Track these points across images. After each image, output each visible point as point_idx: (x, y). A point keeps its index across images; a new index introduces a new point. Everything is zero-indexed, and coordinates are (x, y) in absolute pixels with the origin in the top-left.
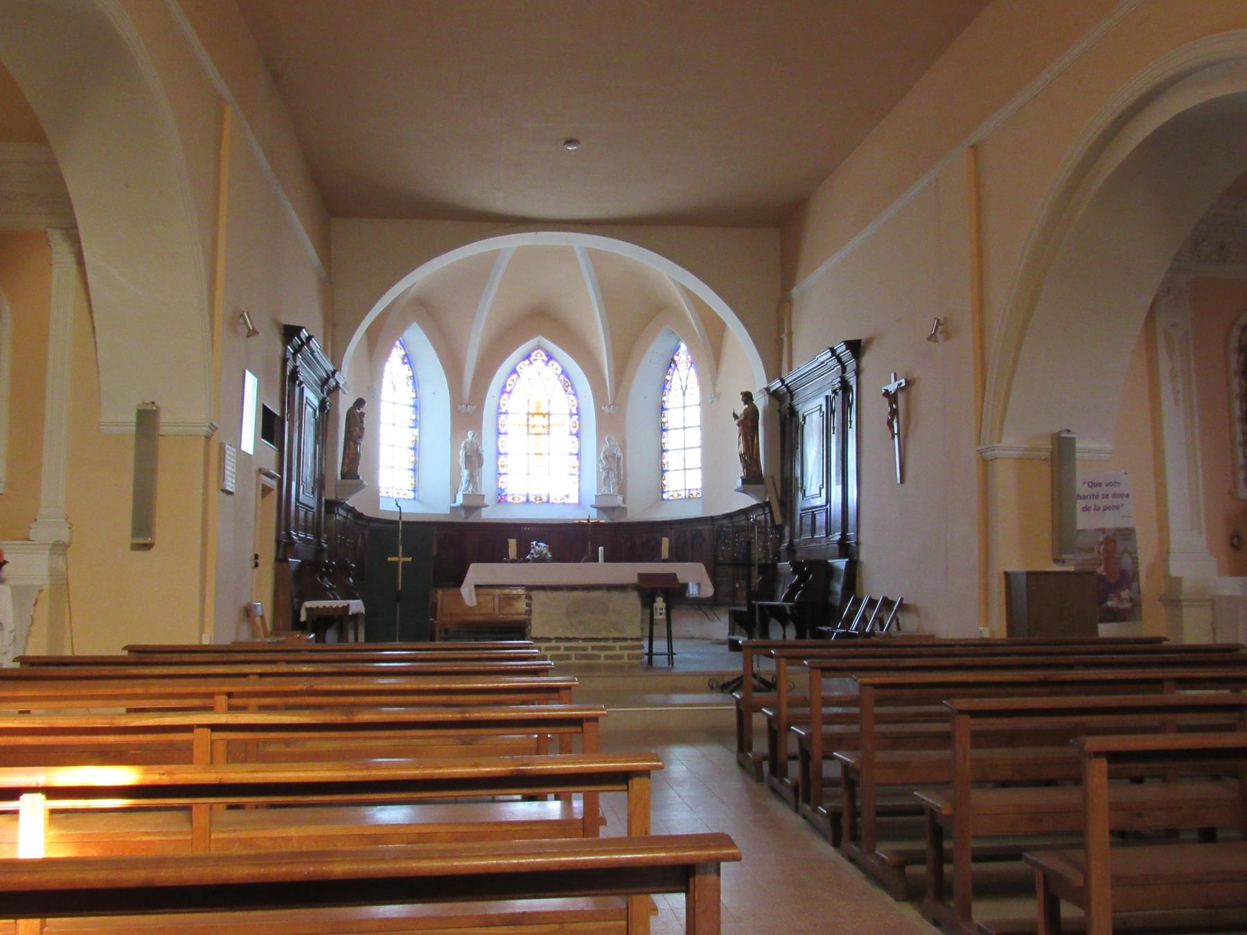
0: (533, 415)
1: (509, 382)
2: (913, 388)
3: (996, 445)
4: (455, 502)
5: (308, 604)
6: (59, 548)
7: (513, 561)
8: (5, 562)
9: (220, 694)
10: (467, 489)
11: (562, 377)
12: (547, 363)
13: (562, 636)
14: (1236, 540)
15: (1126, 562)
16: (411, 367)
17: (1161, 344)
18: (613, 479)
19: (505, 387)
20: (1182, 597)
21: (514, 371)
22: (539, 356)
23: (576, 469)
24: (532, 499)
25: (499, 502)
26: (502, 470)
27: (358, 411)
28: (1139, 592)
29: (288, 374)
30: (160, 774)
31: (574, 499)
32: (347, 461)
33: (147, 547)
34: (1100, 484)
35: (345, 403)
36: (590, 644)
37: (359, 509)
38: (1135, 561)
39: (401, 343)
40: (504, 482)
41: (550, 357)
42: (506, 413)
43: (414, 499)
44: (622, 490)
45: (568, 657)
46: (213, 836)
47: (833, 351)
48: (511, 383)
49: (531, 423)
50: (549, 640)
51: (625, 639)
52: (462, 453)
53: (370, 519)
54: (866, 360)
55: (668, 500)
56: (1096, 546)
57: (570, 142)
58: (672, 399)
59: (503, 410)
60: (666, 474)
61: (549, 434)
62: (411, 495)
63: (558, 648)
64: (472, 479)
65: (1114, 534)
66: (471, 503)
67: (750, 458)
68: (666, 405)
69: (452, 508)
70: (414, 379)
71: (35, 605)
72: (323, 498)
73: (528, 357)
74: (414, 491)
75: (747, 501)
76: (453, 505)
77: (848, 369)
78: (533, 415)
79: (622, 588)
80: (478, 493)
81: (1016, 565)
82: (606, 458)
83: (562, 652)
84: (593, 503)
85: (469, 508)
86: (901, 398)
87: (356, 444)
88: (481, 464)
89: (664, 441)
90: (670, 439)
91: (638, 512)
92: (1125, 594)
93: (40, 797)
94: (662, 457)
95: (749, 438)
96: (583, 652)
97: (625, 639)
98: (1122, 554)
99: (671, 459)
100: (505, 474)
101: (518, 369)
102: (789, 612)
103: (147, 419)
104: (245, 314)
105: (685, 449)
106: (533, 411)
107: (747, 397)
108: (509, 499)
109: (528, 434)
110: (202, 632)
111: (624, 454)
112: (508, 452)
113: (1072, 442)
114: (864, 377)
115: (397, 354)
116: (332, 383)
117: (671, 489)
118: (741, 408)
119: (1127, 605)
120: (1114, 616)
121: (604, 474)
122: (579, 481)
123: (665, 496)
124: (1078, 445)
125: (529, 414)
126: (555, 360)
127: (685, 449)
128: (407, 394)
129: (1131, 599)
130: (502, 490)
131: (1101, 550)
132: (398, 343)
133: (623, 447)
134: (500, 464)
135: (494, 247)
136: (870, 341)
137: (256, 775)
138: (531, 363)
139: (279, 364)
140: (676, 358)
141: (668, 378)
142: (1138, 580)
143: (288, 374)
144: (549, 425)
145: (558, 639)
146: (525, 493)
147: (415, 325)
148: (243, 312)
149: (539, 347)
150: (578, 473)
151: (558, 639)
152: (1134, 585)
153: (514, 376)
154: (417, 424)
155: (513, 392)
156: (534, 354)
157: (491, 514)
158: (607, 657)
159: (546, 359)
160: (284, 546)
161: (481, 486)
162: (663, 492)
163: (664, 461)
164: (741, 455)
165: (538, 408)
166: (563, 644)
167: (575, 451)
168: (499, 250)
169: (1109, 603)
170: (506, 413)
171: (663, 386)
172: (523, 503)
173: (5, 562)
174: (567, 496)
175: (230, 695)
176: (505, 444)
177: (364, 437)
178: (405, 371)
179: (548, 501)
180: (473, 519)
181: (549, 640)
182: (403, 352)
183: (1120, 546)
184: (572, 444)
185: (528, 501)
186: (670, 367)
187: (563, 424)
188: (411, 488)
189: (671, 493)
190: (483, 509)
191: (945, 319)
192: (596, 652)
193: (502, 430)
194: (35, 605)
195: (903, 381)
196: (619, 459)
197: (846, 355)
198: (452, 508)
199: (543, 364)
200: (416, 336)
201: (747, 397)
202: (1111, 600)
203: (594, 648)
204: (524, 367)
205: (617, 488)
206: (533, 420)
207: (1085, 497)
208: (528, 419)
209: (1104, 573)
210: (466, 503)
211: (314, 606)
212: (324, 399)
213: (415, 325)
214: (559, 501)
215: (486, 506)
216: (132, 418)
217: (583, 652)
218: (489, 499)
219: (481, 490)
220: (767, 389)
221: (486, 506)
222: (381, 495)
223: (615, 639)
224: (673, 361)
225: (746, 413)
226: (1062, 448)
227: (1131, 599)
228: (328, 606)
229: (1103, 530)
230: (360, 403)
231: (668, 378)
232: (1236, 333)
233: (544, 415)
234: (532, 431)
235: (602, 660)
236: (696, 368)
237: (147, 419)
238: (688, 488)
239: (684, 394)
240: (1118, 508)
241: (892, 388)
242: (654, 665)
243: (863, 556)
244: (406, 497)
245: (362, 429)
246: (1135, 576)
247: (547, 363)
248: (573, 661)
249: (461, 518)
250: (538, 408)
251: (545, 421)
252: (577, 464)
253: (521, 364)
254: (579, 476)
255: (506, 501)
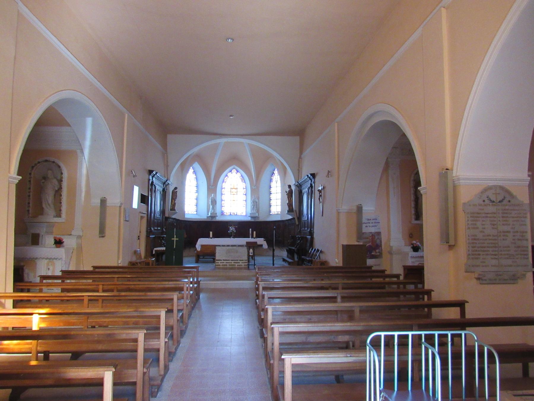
0: (232, 189)
1: (225, 179)
2: (325, 189)
3: (340, 209)
4: (208, 215)
5: (155, 249)
6: (79, 237)
7: (211, 238)
8: (64, 242)
9: (100, 285)
10: (212, 211)
11: (241, 177)
12: (237, 173)
13: (225, 259)
14: (411, 235)
15: (378, 241)
16: (196, 175)
17: (390, 179)
18: (255, 208)
19: (224, 180)
20: (392, 252)
21: (227, 176)
22: (234, 171)
23: (245, 205)
24: (232, 214)
25: (222, 215)
26: (223, 205)
27: (175, 191)
28: (382, 250)
29: (150, 183)
30: (62, 310)
31: (244, 214)
32: (172, 205)
33: (103, 237)
34: (371, 220)
35: (171, 189)
36: (233, 262)
37: (177, 218)
38: (381, 242)
39: (192, 168)
40: (223, 209)
41: (238, 171)
42: (224, 188)
43: (196, 214)
44: (258, 211)
45: (226, 265)
46: (89, 321)
47: (308, 176)
48: (226, 179)
49: (231, 191)
50: (221, 260)
51: (243, 260)
52: (210, 200)
53: (182, 221)
54: (316, 179)
55: (272, 214)
56: (369, 237)
57: (231, 116)
58: (273, 184)
59: (223, 187)
60: (271, 207)
61: (237, 194)
62: (195, 213)
63: (224, 263)
64: (213, 208)
65: (375, 234)
66: (213, 215)
67: (290, 205)
68: (271, 186)
69: (207, 217)
70: (196, 179)
71: (72, 253)
72: (164, 217)
73: (231, 171)
74: (196, 211)
75: (290, 217)
76: (208, 216)
77: (312, 181)
78: (232, 189)
79: (241, 246)
80: (215, 212)
81: (345, 243)
82: (253, 202)
83: (225, 264)
84: (249, 215)
85: (212, 217)
86: (322, 192)
87: (175, 200)
88: (216, 204)
89: (271, 197)
90: (272, 196)
91: (263, 218)
92: (377, 251)
93: (37, 315)
94: (270, 202)
95: (290, 199)
96: (231, 264)
97: (243, 260)
98: (377, 239)
99: (273, 202)
100: (224, 206)
101: (228, 175)
102: (296, 251)
103: (103, 202)
104: (133, 171)
105: (276, 199)
106: (232, 188)
107: (290, 186)
108: (225, 214)
109: (231, 194)
110: (118, 259)
111: (259, 201)
112: (225, 200)
113: (362, 207)
114: (316, 184)
115: (191, 171)
116: (166, 183)
117: (272, 211)
118: (288, 190)
119: (378, 254)
120: (373, 257)
121: (253, 206)
122: (246, 209)
123: (271, 213)
124: (363, 208)
125: (231, 188)
126: (239, 172)
127: (276, 199)
128: (194, 183)
129: (379, 252)
130: (223, 211)
131: (371, 238)
132: (191, 168)
133: (258, 198)
134: (222, 203)
135: (218, 142)
136: (317, 174)
137: (81, 311)
138: (232, 173)
139: (147, 181)
140: (274, 172)
141: (272, 178)
142: (382, 247)
143: (150, 183)
144: (237, 192)
145: (224, 260)
146: (230, 212)
147: (196, 163)
148: (132, 170)
149: (234, 168)
150: (245, 206)
151: (224, 260)
152: (380, 248)
153: (227, 177)
154: (197, 192)
155: (226, 182)
156: (233, 171)
157: (219, 218)
158: (238, 265)
159: (236, 172)
160: (149, 232)
161: (216, 210)
162: (270, 212)
163: (271, 203)
164: (287, 204)
165: (234, 187)
166: (225, 262)
167: (245, 199)
168: (220, 143)
169: (373, 253)
170: (224, 188)
171: (271, 180)
172: (229, 215)
173: (64, 242)
174: (242, 213)
175: (103, 285)
176: (224, 197)
177: (177, 198)
178: (194, 176)
179: (237, 215)
180: (214, 220)
181: (221, 260)
182: (193, 171)
183: (376, 237)
184: (244, 197)
185: (231, 214)
186: (273, 174)
187: (241, 191)
188: (195, 211)
189: (272, 213)
190: (217, 217)
191: (331, 171)
192: (234, 264)
193: (223, 193)
194: (72, 253)
195: (322, 187)
196: (257, 202)
197: (311, 177)
198: (207, 217)
199: (236, 174)
200: (197, 165)
201: (290, 186)
202: (373, 252)
203: (234, 263)
204: (229, 174)
205: (256, 211)
206: (232, 190)
207: (366, 223)
208: (231, 190)
209: (371, 245)
210: (212, 215)
211: (157, 249)
212: (164, 188)
213: (196, 163)
214: (240, 214)
215: (217, 216)
216: (100, 201)
217: (231, 264)
218: (219, 214)
219: (216, 212)
220: (295, 184)
221: (217, 216)
222: (186, 213)
223: (240, 260)
224: (273, 173)
225: (289, 191)
226: (360, 209)
227: (379, 252)
228: (161, 249)
229: (371, 233)
230: (176, 188)
231: (272, 178)
232: (413, 176)
233: (236, 189)
234: (232, 193)
235: (236, 266)
236: (279, 175)
237: (103, 202)
238: (277, 211)
239: (277, 183)
240: (376, 226)
241: (320, 188)
242: (250, 268)
243: (315, 236)
244: (194, 213)
245: (176, 196)
246: (381, 246)
247: (237, 173)
248: (228, 266)
249: (210, 220)
250: (234, 187)
251: (236, 191)
252: (245, 203)
253: (229, 174)
254: (246, 207)
255: (224, 215)
